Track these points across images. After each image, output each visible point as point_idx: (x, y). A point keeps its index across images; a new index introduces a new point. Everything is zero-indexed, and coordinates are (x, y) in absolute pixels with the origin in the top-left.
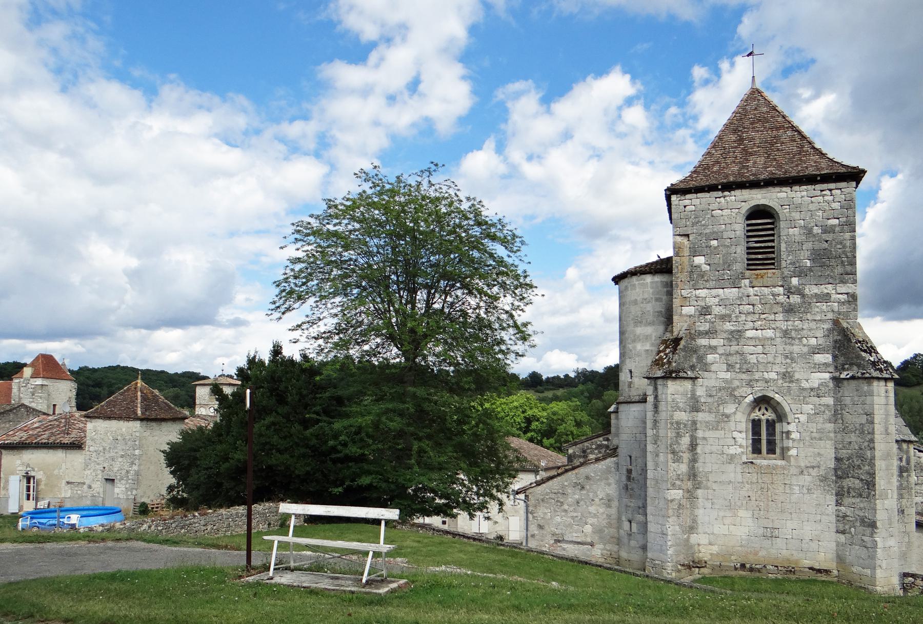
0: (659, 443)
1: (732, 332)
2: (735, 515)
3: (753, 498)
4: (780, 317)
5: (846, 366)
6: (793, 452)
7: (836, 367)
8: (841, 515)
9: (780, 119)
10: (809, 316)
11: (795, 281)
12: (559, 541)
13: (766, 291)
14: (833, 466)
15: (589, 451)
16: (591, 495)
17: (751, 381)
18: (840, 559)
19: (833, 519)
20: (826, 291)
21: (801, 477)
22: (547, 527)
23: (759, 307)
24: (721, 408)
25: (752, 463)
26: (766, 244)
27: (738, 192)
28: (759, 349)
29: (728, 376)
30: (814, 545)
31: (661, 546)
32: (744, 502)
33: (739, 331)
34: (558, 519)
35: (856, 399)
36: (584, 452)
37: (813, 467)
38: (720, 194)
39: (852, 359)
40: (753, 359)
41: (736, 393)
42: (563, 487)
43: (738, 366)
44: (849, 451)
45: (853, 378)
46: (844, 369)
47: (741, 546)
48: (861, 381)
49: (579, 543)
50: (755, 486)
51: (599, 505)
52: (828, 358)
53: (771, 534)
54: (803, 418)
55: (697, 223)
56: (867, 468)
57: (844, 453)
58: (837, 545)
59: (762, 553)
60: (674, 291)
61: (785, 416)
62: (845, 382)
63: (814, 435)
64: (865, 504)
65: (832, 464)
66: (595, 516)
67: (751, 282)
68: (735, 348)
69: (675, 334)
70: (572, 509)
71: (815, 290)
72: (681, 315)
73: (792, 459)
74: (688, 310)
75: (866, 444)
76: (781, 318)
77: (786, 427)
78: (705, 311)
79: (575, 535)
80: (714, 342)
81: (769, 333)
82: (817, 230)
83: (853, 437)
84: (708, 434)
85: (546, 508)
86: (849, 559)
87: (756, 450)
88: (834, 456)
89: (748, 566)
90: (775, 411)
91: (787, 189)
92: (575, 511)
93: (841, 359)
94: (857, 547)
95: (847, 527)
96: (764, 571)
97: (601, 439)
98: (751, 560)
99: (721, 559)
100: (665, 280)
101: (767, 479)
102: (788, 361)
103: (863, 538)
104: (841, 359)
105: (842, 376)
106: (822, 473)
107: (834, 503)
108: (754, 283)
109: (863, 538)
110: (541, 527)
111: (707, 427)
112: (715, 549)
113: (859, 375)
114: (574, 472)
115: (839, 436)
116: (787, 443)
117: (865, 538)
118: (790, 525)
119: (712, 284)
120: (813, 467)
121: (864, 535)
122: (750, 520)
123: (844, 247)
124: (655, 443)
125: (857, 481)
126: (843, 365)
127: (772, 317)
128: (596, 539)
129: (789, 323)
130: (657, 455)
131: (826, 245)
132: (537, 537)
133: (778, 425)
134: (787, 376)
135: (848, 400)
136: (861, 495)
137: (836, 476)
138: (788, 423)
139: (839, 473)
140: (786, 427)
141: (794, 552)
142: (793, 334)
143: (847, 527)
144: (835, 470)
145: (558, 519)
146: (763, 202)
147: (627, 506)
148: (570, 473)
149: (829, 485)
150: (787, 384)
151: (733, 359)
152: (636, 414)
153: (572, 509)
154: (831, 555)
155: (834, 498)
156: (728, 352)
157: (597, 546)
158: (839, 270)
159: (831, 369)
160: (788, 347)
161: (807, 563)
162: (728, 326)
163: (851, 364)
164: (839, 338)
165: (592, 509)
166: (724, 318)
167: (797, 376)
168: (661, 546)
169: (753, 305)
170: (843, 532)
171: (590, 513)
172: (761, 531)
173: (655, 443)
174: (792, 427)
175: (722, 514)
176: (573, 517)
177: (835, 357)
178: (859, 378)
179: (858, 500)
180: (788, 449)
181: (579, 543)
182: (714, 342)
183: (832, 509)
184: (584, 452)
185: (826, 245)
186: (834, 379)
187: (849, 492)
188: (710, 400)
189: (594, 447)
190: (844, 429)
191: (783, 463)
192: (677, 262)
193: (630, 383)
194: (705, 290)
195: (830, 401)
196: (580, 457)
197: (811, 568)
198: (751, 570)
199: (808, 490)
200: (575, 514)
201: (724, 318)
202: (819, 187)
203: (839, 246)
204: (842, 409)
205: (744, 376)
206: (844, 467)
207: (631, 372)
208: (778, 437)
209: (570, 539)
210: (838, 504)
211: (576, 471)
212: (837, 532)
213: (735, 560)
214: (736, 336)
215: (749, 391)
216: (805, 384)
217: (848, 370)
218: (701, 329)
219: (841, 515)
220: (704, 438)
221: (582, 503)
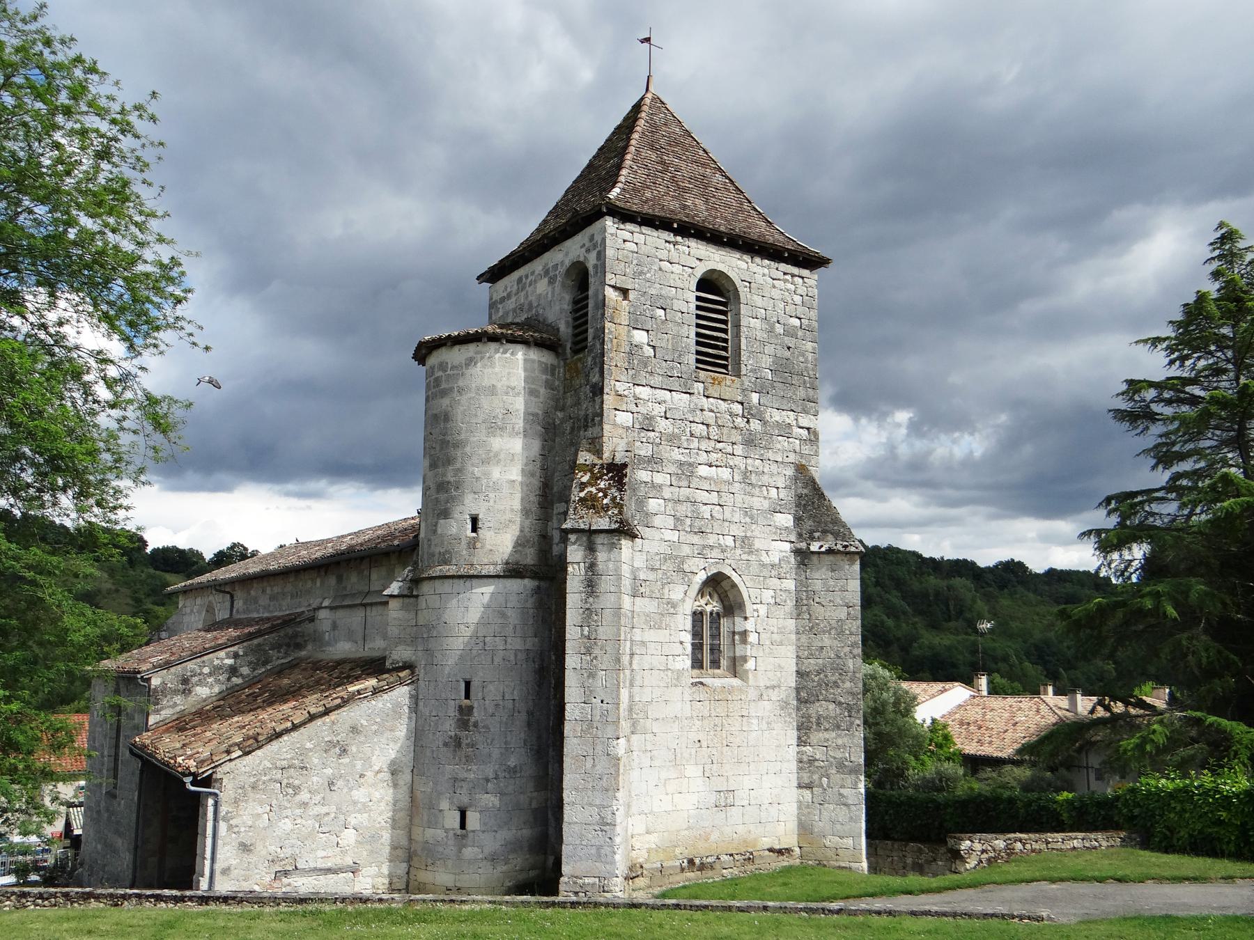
0: (596, 651)
1: (681, 464)
2: (682, 776)
3: (704, 744)
4: (739, 450)
5: (817, 535)
6: (750, 665)
7: (800, 535)
8: (805, 758)
9: (701, 152)
10: (770, 455)
11: (755, 397)
12: (286, 873)
13: (723, 406)
14: (794, 685)
15: (195, 679)
16: (359, 764)
17: (704, 547)
18: (804, 829)
19: (793, 766)
20: (788, 421)
21: (761, 703)
22: (259, 847)
23: (714, 432)
24: (666, 591)
25: (701, 683)
26: (715, 334)
27: (693, 243)
28: (714, 498)
29: (674, 536)
30: (773, 810)
31: (599, 848)
32: (693, 751)
33: (690, 465)
34: (287, 825)
35: (832, 583)
36: (185, 681)
37: (773, 687)
38: (671, 237)
39: (826, 523)
40: (705, 511)
41: (686, 567)
42: (303, 752)
43: (688, 521)
44: (820, 661)
45: (830, 551)
46: (812, 539)
47: (688, 828)
48: (839, 557)
49: (329, 871)
50: (706, 722)
51: (373, 785)
52: (786, 520)
53: (724, 801)
54: (763, 610)
55: (641, 273)
56: (848, 685)
57: (811, 664)
58: (799, 808)
59: (714, 836)
60: (606, 381)
61: (741, 606)
62: (815, 558)
63: (775, 636)
64: (845, 740)
65: (792, 681)
66: (365, 808)
67: (705, 389)
68: (685, 492)
69: (606, 455)
70: (318, 798)
71: (777, 416)
72: (615, 425)
73: (750, 676)
74: (624, 418)
75: (847, 649)
76: (740, 453)
77: (740, 625)
78: (647, 425)
79: (321, 853)
80: (659, 478)
81: (725, 473)
82: (779, 329)
83: (827, 641)
84: (650, 635)
85: (261, 803)
86: (819, 826)
87: (697, 663)
88: (795, 669)
89: (697, 861)
90: (723, 599)
91: (747, 258)
92: (323, 802)
93: (809, 524)
94: (831, 807)
95: (816, 777)
96: (717, 866)
97: (222, 654)
98: (701, 851)
99: (662, 856)
100: (543, 360)
101: (720, 709)
102: (748, 520)
103: (842, 791)
104: (809, 524)
105: (815, 547)
106: (783, 696)
107: (794, 742)
108: (711, 392)
109: (842, 791)
110: (245, 848)
111: (646, 622)
112: (653, 840)
113: (839, 547)
114: (327, 719)
115: (804, 638)
116: (739, 651)
117: (844, 791)
118: (747, 782)
119: (656, 381)
120: (773, 687)
121: (843, 787)
122: (700, 781)
123: (806, 361)
124: (588, 652)
125: (832, 706)
126: (811, 532)
127: (729, 449)
128: (363, 855)
129: (749, 461)
130: (592, 675)
131: (787, 354)
132: (234, 873)
133: (725, 623)
134: (745, 542)
135: (818, 585)
136: (838, 727)
137: (798, 700)
138: (746, 618)
139: (803, 694)
140: (740, 625)
141: (752, 827)
142: (754, 478)
143: (816, 777)
144: (798, 690)
145: (287, 825)
146: (720, 267)
147: (455, 780)
148: (319, 722)
149: (790, 714)
150: (745, 557)
151: (684, 509)
152: (486, 598)
153: (318, 798)
154: (793, 825)
155: (795, 733)
156: (676, 498)
157: (364, 871)
158: (801, 393)
159: (793, 538)
160: (747, 498)
161: (767, 842)
162: (676, 455)
163: (824, 532)
164: (805, 491)
165: (359, 795)
166: (673, 439)
167: (758, 544)
168: (599, 848)
169: (708, 425)
170: (809, 787)
171: (355, 803)
172: (712, 798)
173: (588, 652)
174: (749, 625)
175: (664, 775)
176: (318, 817)
177: (798, 520)
178: (839, 552)
179: (834, 734)
180: (744, 659)
181: (329, 871)
182: (659, 478)
183: (793, 750)
184: (185, 681)
185: (787, 354)
186: (797, 552)
187: (818, 724)
188: (651, 576)
189: (206, 670)
190: (811, 629)
191: (736, 682)
192: (611, 332)
193: (475, 540)
194: (648, 389)
195: (790, 584)
196: (176, 692)
197: (771, 850)
198: (702, 867)
199: (768, 723)
200: (325, 810)
201: (673, 439)
202: (783, 267)
203: (801, 359)
204: (808, 598)
205: (696, 539)
206: (810, 685)
207: (475, 520)
208: (724, 641)
209: (312, 865)
210: (801, 742)
211: (333, 716)
212: (800, 787)
213: (682, 853)
214: (686, 471)
215: (702, 563)
216: (765, 559)
217: (819, 539)
218: (642, 453)
219: (805, 758)
220: (643, 643)
221: (340, 783)
